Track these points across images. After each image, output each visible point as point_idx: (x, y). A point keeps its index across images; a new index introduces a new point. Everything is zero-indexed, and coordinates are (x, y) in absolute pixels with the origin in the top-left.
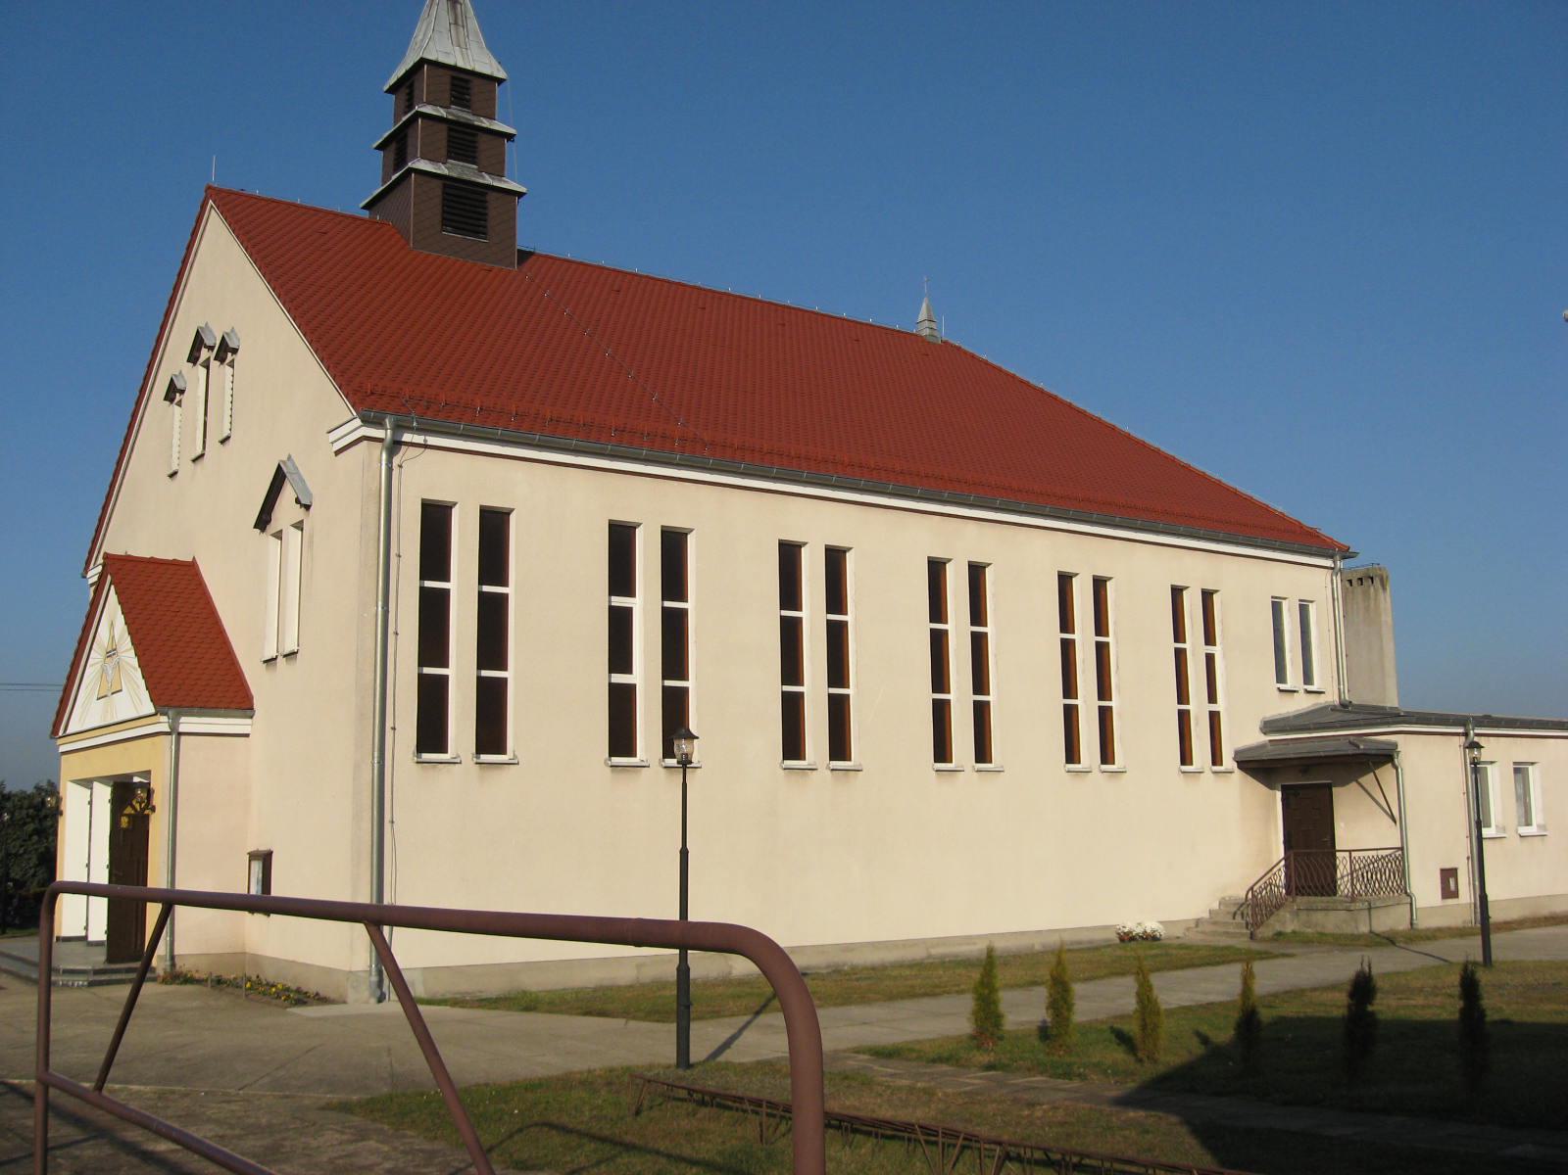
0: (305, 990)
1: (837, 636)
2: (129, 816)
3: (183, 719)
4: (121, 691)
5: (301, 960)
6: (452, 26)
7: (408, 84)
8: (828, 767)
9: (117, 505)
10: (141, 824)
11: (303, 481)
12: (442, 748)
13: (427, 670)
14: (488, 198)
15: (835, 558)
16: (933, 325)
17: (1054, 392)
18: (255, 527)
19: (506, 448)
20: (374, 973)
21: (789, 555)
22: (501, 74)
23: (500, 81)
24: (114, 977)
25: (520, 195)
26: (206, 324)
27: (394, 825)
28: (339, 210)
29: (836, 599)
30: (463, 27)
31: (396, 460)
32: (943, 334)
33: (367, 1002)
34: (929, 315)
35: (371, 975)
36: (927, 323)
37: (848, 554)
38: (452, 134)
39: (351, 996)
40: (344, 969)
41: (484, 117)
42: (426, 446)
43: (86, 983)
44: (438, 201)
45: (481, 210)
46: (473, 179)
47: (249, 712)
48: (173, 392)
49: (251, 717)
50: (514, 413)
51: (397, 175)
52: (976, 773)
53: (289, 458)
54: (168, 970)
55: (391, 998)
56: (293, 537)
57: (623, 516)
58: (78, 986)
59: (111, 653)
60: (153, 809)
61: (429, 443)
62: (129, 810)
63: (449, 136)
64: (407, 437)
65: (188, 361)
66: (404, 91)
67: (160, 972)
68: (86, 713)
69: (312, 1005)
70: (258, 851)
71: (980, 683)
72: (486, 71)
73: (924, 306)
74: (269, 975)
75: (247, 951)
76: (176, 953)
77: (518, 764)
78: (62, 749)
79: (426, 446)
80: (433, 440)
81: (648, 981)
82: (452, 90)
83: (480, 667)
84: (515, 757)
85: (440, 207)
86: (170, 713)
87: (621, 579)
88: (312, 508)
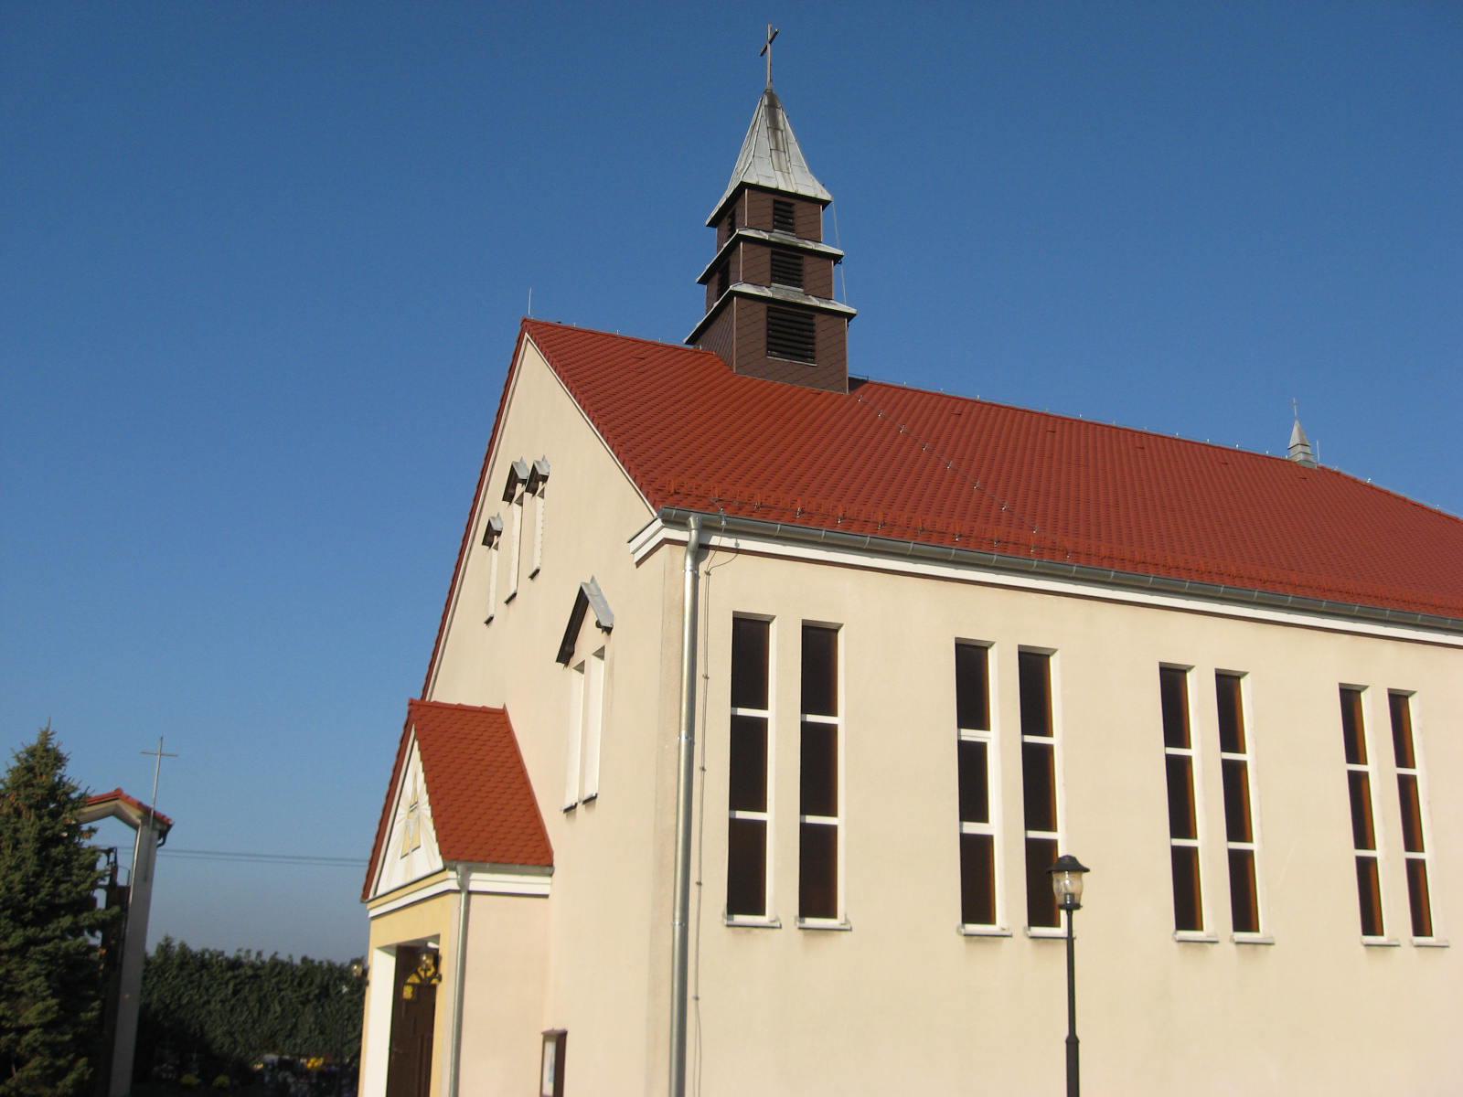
1: (1234, 777)
2: (413, 985)
3: (474, 876)
4: (419, 847)
6: (773, 152)
7: (730, 213)
8: (1232, 940)
10: (427, 993)
11: (605, 602)
12: (759, 909)
14: (795, 208)
15: (1228, 686)
16: (1308, 450)
17: (1454, 514)
18: (557, 661)
21: (1173, 681)
22: (825, 196)
23: (825, 203)
25: (850, 316)
26: (521, 460)
27: (700, 1002)
28: (659, 341)
29: (1231, 735)
30: (785, 152)
31: (703, 567)
32: (1318, 460)
34: (1302, 440)
36: (1300, 448)
37: (1242, 681)
38: (776, 257)
41: (808, 240)
42: (737, 551)
44: (762, 325)
45: (808, 334)
46: (799, 301)
48: (491, 536)
49: (551, 875)
50: (840, 515)
51: (717, 303)
52: (1415, 950)
56: (597, 668)
57: (972, 634)
59: (414, 807)
60: (440, 979)
61: (741, 547)
62: (414, 979)
63: (773, 260)
64: (715, 540)
65: (504, 500)
66: (726, 221)
68: (393, 874)
70: (553, 1030)
71: (1412, 838)
72: (810, 193)
73: (1295, 429)
77: (851, 930)
78: (372, 913)
79: (737, 551)
80: (746, 544)
82: (774, 214)
83: (804, 811)
84: (847, 921)
85: (764, 331)
86: (460, 867)
87: (972, 708)
88: (613, 631)
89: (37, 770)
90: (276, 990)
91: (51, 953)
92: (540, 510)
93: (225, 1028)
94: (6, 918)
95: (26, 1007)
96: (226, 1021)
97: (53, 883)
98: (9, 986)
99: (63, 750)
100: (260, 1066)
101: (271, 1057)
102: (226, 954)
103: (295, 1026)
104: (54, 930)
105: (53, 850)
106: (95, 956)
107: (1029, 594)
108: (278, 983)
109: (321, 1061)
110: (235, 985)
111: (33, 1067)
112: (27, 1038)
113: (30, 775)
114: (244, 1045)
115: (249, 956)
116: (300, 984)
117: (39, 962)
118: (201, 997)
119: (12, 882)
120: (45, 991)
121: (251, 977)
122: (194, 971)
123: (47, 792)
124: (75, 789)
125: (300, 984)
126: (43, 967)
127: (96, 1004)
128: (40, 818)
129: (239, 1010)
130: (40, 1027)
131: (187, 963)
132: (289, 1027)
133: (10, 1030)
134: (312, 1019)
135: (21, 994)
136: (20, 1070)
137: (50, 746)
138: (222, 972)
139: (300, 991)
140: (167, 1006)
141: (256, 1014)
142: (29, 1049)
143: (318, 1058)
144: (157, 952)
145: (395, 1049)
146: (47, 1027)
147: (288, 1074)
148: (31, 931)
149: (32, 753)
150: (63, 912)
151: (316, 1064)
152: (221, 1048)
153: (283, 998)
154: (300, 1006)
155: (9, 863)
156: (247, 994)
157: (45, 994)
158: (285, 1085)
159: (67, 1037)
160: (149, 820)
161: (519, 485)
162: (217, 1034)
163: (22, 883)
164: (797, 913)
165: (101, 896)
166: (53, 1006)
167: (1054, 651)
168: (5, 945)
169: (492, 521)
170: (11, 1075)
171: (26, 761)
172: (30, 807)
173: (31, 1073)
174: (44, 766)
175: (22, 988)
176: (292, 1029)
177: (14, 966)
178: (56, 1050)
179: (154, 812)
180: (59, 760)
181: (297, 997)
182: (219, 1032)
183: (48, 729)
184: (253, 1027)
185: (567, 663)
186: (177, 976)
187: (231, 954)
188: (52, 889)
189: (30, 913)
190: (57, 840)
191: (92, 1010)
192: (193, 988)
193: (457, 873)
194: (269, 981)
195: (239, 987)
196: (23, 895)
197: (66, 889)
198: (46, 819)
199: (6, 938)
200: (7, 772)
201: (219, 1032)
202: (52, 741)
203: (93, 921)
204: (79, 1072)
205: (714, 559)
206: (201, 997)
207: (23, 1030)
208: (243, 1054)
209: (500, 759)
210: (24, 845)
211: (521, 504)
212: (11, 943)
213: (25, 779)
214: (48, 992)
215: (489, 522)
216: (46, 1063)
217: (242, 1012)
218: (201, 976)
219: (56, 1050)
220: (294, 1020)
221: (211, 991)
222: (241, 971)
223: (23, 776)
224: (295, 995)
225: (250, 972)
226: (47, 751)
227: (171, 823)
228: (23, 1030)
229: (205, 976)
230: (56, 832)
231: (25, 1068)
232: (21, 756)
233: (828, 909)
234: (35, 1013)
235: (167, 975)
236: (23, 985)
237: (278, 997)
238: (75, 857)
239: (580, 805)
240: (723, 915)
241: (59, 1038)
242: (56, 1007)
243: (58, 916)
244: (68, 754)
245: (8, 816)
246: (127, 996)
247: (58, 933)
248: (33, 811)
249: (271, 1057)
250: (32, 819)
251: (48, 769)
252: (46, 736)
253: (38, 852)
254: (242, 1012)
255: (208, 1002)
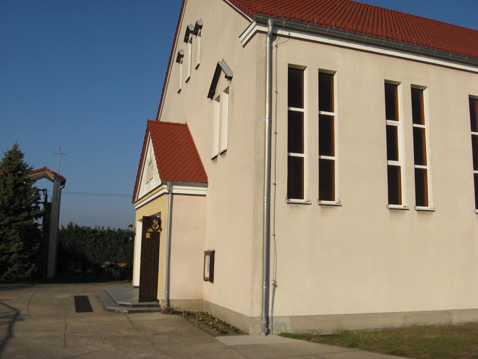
0: (228, 323)
2: (150, 232)
3: (175, 187)
4: (153, 178)
5: (227, 307)
9: (162, 115)
10: (156, 236)
13: (292, 154)
19: (331, 40)
20: (264, 319)
24: (141, 309)
31: (274, 43)
33: (260, 335)
35: (262, 320)
39: (251, 331)
40: (248, 315)
42: (289, 37)
43: (127, 312)
47: (205, 184)
49: (207, 187)
53: (223, 60)
54: (166, 306)
55: (273, 333)
56: (225, 98)
57: (392, 78)
58: (124, 312)
59: (150, 163)
60: (161, 230)
62: (150, 230)
64: (279, 32)
65: (184, 42)
67: (162, 307)
68: (143, 190)
69: (230, 335)
74: (213, 312)
75: (204, 299)
76: (170, 298)
78: (136, 207)
79: (289, 37)
80: (293, 34)
81: (409, 325)
86: (168, 183)
89: (13, 159)
90: (109, 240)
91: (20, 225)
92: (199, 41)
93: (92, 254)
94: (2, 213)
95: (12, 245)
96: (92, 251)
97: (20, 200)
98: (5, 238)
99: (22, 152)
100: (104, 266)
101: (107, 263)
102: (91, 228)
103: (116, 252)
104: (21, 217)
105: (20, 188)
106: (39, 227)
107: (415, 63)
108: (110, 238)
109: (125, 264)
110: (95, 239)
111: (15, 267)
112: (13, 257)
113: (10, 161)
114: (99, 259)
115: (100, 229)
116: (117, 238)
117: (15, 229)
118: (83, 243)
119: (4, 200)
120: (19, 239)
121: (100, 236)
122: (80, 234)
123: (16, 167)
124: (27, 166)
125: (117, 238)
126: (17, 231)
127: (38, 244)
128: (14, 176)
129: (96, 247)
130: (17, 253)
131: (78, 231)
132: (114, 253)
133: (6, 254)
134: (122, 250)
135: (10, 241)
136: (10, 268)
137: (18, 150)
138: (90, 234)
139: (117, 241)
140: (72, 246)
141: (102, 248)
142: (14, 260)
143: (124, 263)
144: (68, 227)
145: (143, 259)
146: (20, 253)
147: (112, 269)
148: (12, 218)
149: (10, 153)
150: (24, 211)
151: (123, 265)
152: (91, 260)
153: (112, 243)
154: (117, 246)
155: (3, 193)
156: (99, 242)
157: (19, 240)
158: (112, 272)
159: (28, 256)
160: (57, 179)
161: (191, 34)
162: (89, 255)
163: (8, 200)
164: (318, 198)
165: (42, 206)
166: (22, 245)
167: (425, 88)
168: (3, 223)
169: (180, 52)
170: (7, 270)
171: (9, 155)
172: (10, 172)
173: (15, 269)
174: (15, 157)
175: (10, 238)
176: (115, 253)
177: (6, 231)
178: (23, 261)
179: (59, 175)
180: (21, 155)
181: (117, 243)
182: (90, 254)
183: (16, 144)
184: (101, 253)
185: (212, 98)
186: (74, 236)
187: (93, 228)
188: (19, 202)
189: (12, 211)
190: (21, 184)
191: (37, 246)
192: (80, 240)
193: (167, 186)
194: (107, 237)
195: (96, 239)
196: (9, 204)
197: (25, 202)
198: (17, 177)
199: (3, 220)
200: (2, 160)
201: (90, 254)
202: (18, 149)
203: (35, 214)
204: (33, 269)
205: (279, 40)
206: (83, 243)
207: (11, 254)
208: (99, 262)
209: (185, 142)
210: (8, 186)
211: (191, 43)
212: (5, 222)
213: (8, 162)
214: (20, 240)
215: (179, 52)
216: (20, 266)
217: (97, 247)
218: (83, 235)
219: (23, 261)
220: (116, 250)
221: (87, 241)
222: (97, 234)
223: (8, 161)
224: (115, 242)
225: (100, 234)
226: (16, 152)
227: (65, 179)
228: (11, 254)
229: (84, 235)
230: (21, 181)
231: (12, 268)
232: (6, 154)
233: (331, 197)
234: (15, 247)
235: (71, 235)
236: (10, 237)
237: (110, 243)
238: (28, 191)
239: (219, 155)
240: (286, 198)
241: (25, 257)
242: (23, 245)
243: (22, 212)
244: (251, 315)
245: (3, 176)
246: (52, 242)
247: (23, 218)
248: (11, 173)
249: (107, 263)
250: (11, 177)
251: (17, 159)
252: (16, 147)
253: (14, 189)
254: (97, 247)
255: (86, 244)
